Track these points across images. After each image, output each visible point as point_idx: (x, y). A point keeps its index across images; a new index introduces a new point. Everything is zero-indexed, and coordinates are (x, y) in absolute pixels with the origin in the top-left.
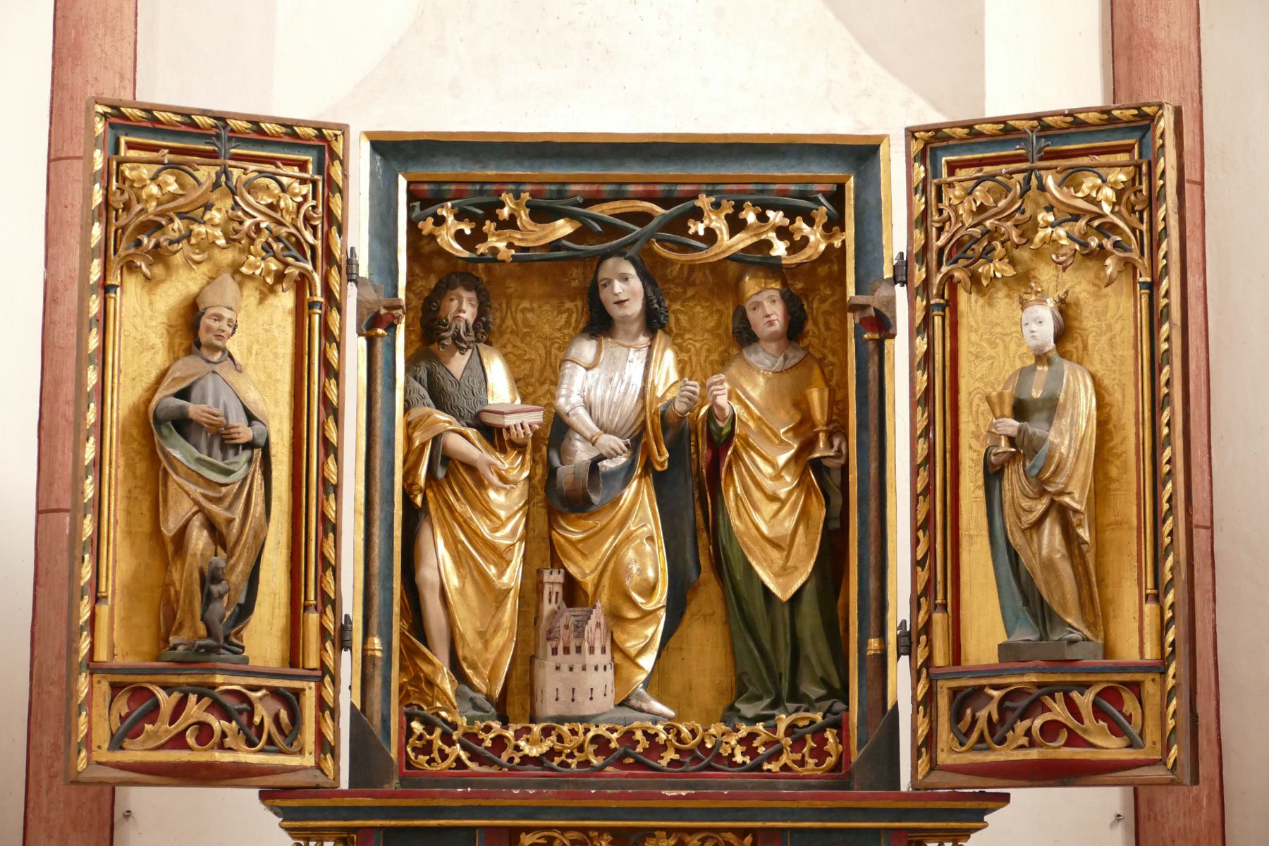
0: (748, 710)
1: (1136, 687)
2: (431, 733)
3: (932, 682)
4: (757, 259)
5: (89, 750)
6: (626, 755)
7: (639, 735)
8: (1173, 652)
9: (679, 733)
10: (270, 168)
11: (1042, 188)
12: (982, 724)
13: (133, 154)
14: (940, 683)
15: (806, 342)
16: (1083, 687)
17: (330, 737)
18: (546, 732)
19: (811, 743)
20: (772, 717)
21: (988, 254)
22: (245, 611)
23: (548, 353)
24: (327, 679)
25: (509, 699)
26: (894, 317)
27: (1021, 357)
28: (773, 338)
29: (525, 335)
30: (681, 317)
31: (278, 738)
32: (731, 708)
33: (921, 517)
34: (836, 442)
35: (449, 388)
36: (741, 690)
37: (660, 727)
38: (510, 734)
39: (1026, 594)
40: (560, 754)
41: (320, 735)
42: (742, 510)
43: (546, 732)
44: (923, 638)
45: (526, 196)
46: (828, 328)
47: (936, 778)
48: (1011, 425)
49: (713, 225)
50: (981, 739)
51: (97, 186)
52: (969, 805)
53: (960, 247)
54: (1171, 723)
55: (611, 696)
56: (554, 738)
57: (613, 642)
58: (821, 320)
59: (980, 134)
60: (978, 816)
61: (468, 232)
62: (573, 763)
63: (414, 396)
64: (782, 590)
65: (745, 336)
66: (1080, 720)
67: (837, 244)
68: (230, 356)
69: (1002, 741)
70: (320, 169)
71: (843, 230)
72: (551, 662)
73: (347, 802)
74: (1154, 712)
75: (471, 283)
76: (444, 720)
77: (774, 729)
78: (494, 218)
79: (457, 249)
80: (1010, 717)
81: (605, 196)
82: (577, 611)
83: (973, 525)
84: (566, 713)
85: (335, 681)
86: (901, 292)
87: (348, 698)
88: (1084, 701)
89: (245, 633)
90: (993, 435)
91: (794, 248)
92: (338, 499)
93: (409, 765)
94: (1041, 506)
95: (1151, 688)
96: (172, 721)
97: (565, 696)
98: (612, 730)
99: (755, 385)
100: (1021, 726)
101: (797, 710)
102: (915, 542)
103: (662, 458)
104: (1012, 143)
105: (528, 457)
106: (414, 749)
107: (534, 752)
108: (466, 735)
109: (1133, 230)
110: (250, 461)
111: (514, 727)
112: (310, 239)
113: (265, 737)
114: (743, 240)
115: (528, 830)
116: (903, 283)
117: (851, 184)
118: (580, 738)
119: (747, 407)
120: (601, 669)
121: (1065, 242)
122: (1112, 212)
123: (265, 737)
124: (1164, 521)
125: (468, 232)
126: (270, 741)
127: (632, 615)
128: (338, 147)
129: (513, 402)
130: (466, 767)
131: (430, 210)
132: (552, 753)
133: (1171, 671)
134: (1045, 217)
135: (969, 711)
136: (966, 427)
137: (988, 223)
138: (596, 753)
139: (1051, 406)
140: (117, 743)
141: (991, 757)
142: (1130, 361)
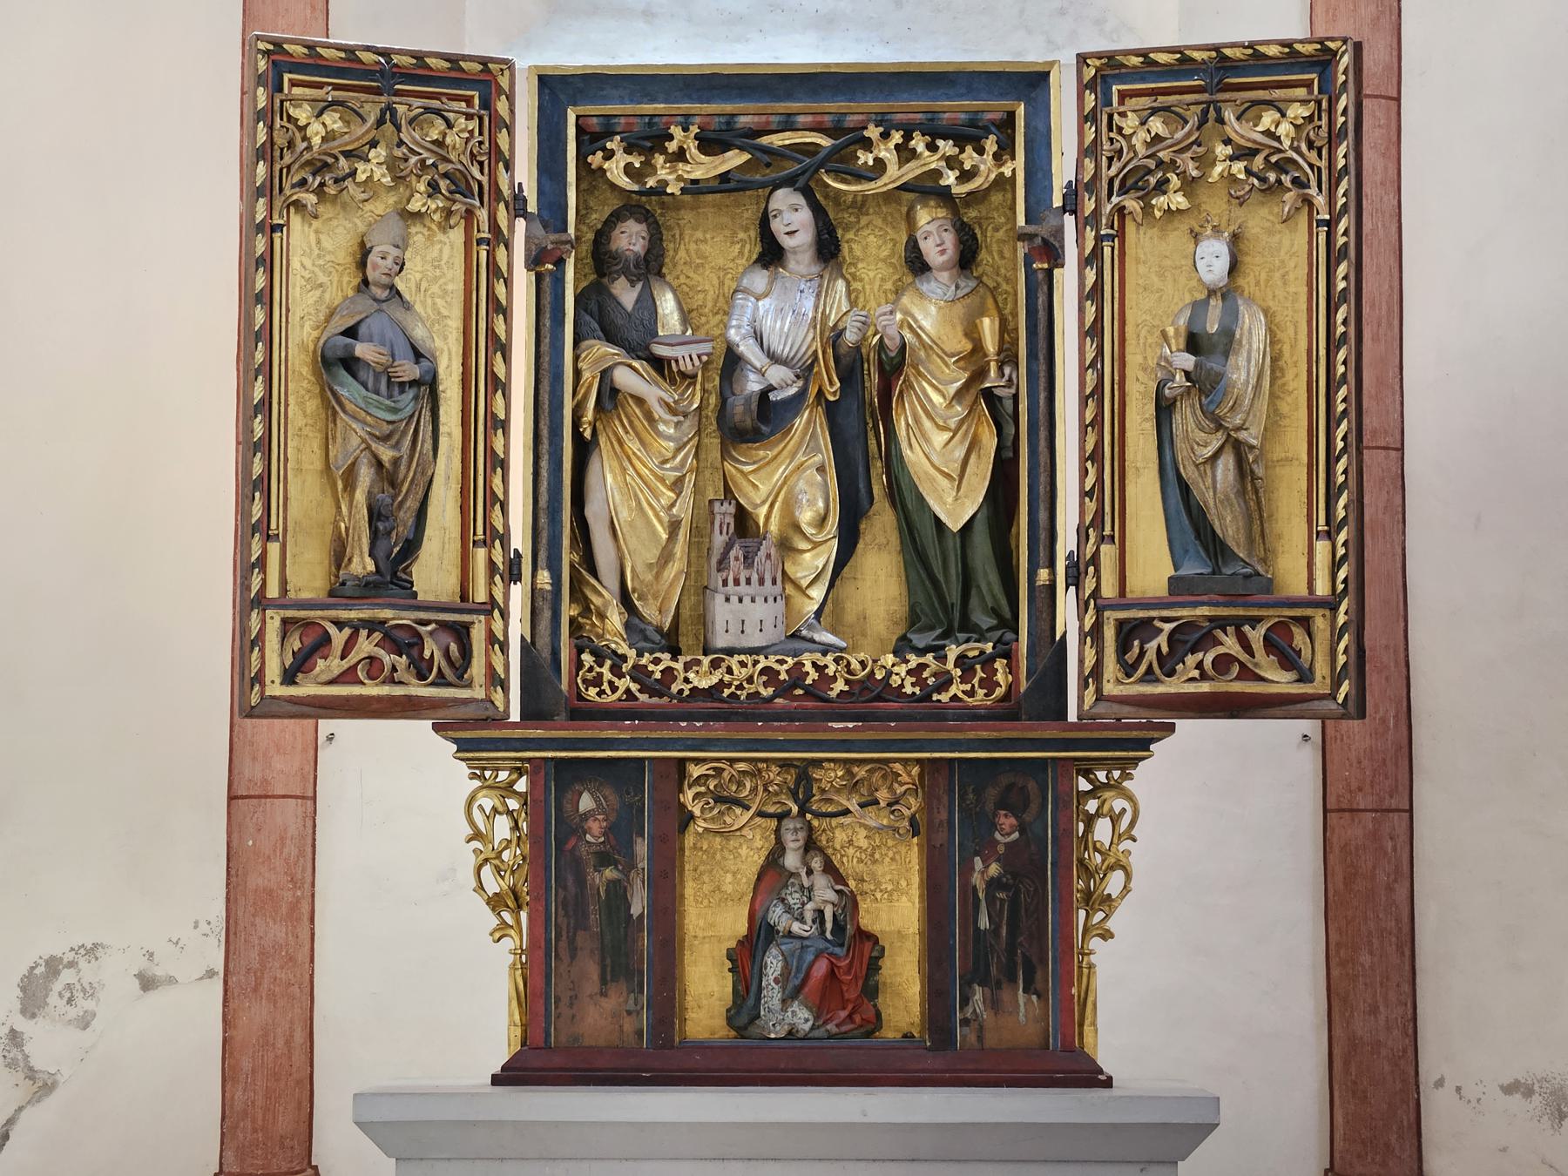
0: (920, 640)
1: (1305, 623)
2: (601, 666)
3: (1099, 611)
4: (927, 189)
5: (263, 685)
6: (795, 686)
7: (808, 667)
8: (1345, 589)
9: (849, 664)
10: (435, 104)
11: (1221, 120)
12: (1151, 655)
13: (297, 91)
14: (1106, 614)
15: (980, 270)
16: (1254, 621)
17: (500, 670)
18: (715, 665)
19: (980, 674)
20: (943, 647)
21: (1162, 187)
22: (411, 547)
23: (722, 283)
24: (496, 613)
25: (682, 628)
26: (1063, 247)
27: (1190, 291)
28: (943, 268)
29: (698, 266)
30: (854, 246)
31: (447, 671)
32: (903, 638)
33: (1090, 447)
34: (1007, 370)
35: (620, 322)
36: (914, 619)
37: (830, 657)
38: (679, 666)
39: (1190, 520)
40: (729, 685)
41: (490, 667)
42: (913, 440)
43: (715, 665)
44: (1091, 569)
45: (695, 130)
46: (1002, 257)
47: (1102, 708)
48: (1188, 361)
49: (882, 154)
50: (1150, 670)
51: (261, 124)
52: (1134, 734)
53: (1133, 182)
54: (1341, 659)
55: (781, 627)
56: (723, 669)
57: (784, 572)
58: (995, 247)
59: (1156, 63)
60: (1144, 745)
61: (637, 165)
62: (743, 695)
63: (584, 329)
64: (954, 524)
65: (917, 264)
66: (1252, 655)
67: (1008, 173)
68: (398, 292)
69: (1171, 673)
70: (486, 104)
71: (1013, 158)
72: (720, 598)
73: (518, 733)
74: (1322, 650)
75: (645, 216)
76: (614, 652)
77: (942, 659)
78: (664, 151)
79: (624, 182)
80: (1181, 649)
81: (774, 127)
82: (749, 542)
83: (1139, 457)
84: (737, 645)
85: (505, 615)
86: (1069, 220)
87: (517, 629)
88: (1256, 636)
89: (414, 569)
90: (1166, 365)
91: (965, 176)
92: (506, 434)
93: (580, 697)
94: (1216, 441)
95: (1320, 623)
96: (343, 658)
97: (734, 628)
98: (782, 662)
99: (927, 314)
100: (1191, 660)
101: (967, 641)
102: (1084, 473)
103: (832, 391)
104: (1188, 74)
105: (698, 387)
106: (584, 681)
107: (704, 684)
108: (634, 667)
109: (1311, 166)
110: (416, 398)
111: (682, 659)
112: (478, 175)
113: (435, 670)
114: (912, 171)
115: (697, 761)
116: (1074, 212)
117: (1021, 111)
118: (750, 669)
119: (918, 336)
120: (771, 600)
121: (1242, 176)
122: (1291, 147)
123: (435, 670)
124: (1338, 459)
125: (637, 165)
126: (440, 673)
127: (803, 545)
128: (504, 82)
129: (684, 333)
130: (636, 699)
131: (599, 144)
132: (721, 685)
133: (1343, 608)
134: (1222, 151)
135: (1136, 643)
136: (1133, 359)
137: (1161, 154)
138: (765, 685)
139: (1227, 341)
140: (289, 677)
141: (1159, 689)
142: (1304, 298)
